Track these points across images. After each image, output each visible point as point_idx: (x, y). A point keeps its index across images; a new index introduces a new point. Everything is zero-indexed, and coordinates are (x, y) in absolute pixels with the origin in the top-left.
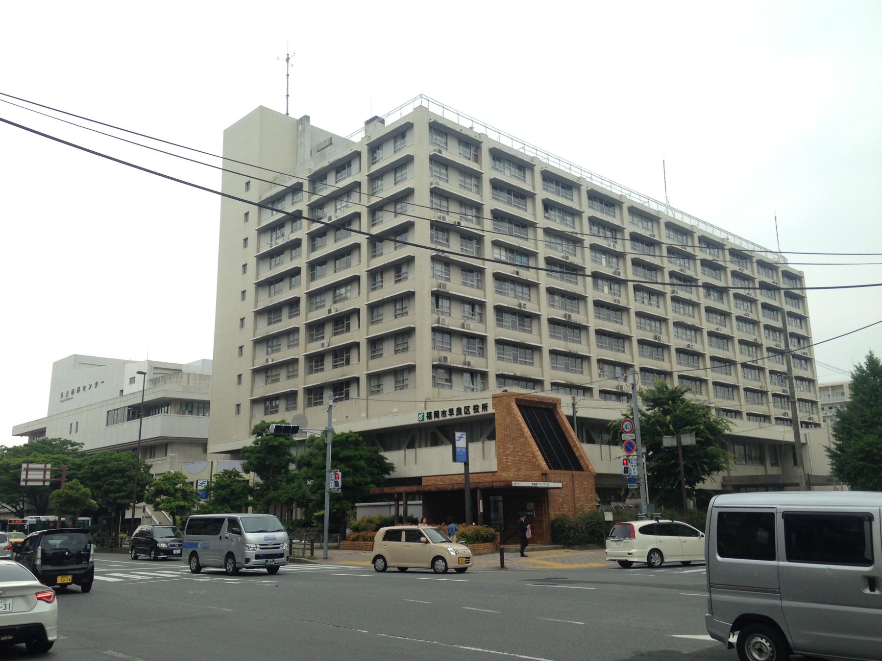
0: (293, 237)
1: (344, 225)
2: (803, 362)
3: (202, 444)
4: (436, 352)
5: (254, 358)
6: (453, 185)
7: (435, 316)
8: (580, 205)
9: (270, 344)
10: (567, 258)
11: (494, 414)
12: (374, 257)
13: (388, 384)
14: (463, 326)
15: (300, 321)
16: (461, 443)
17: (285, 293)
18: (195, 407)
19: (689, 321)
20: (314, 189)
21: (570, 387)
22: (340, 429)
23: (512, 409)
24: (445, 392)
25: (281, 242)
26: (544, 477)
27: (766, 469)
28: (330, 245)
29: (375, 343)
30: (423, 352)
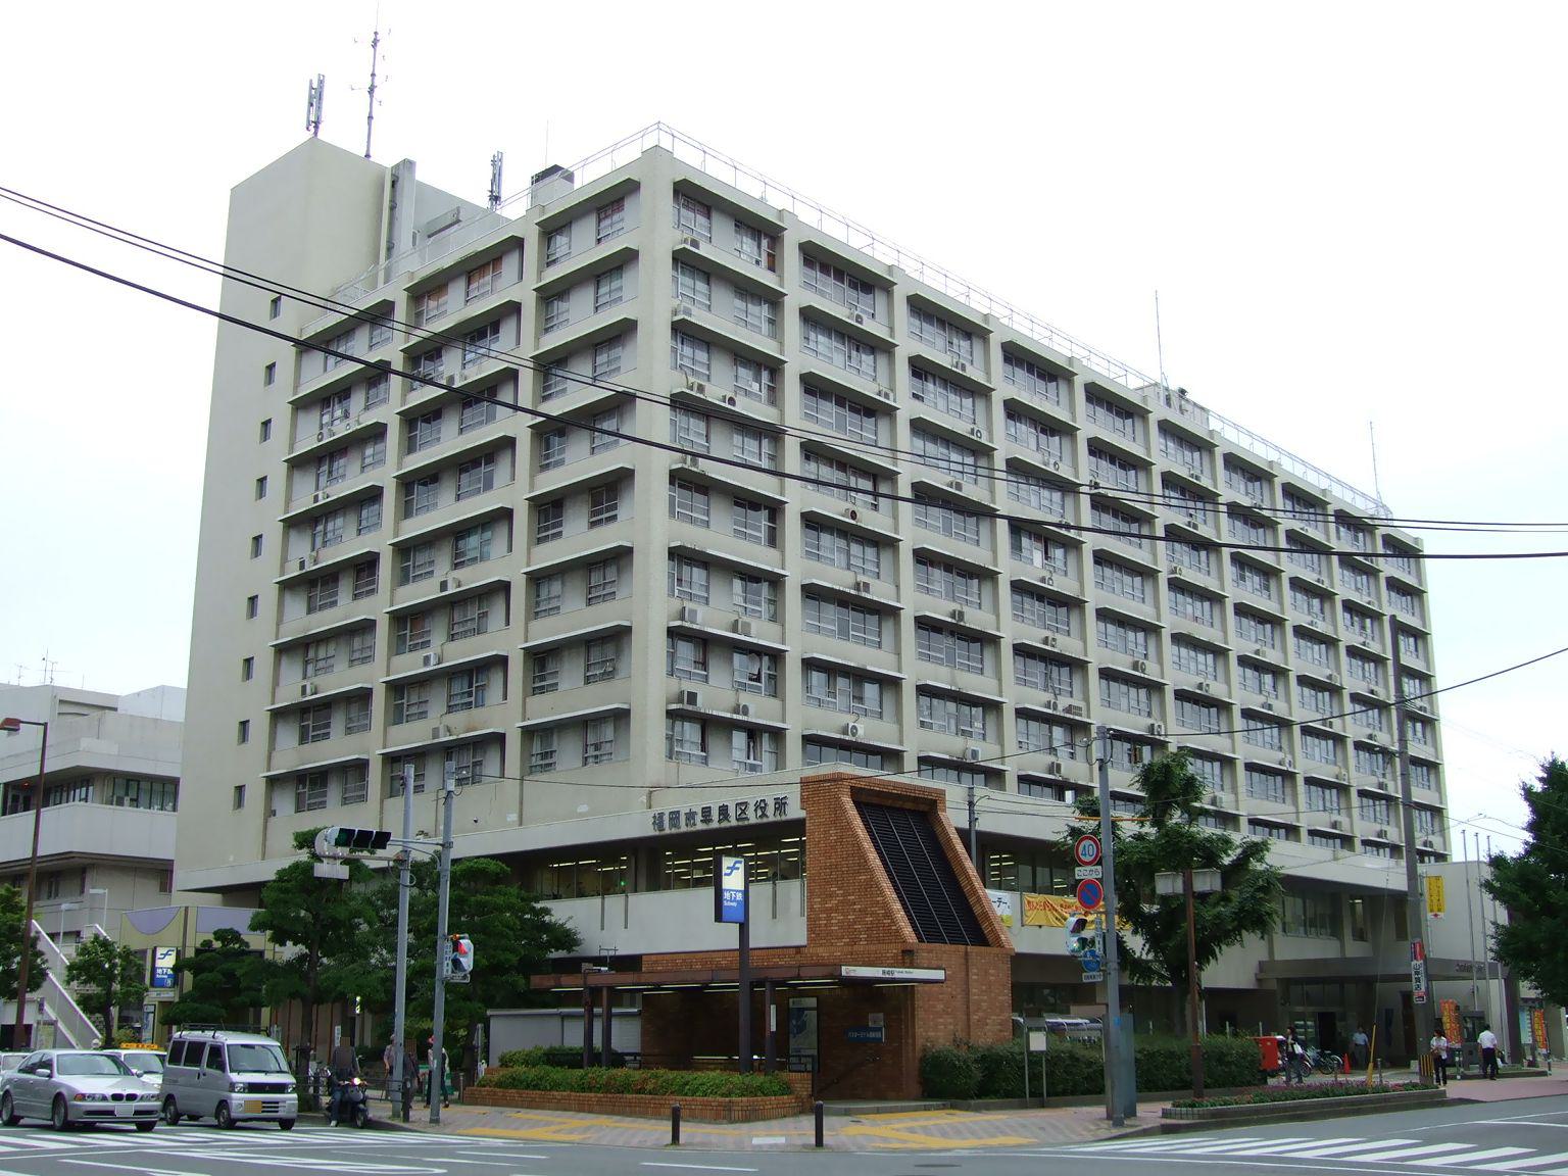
0: (369, 419)
1: (483, 394)
2: (1419, 726)
3: (160, 872)
4: (674, 681)
5: (276, 683)
6: (723, 316)
7: (676, 604)
8: (988, 373)
9: (311, 654)
10: (959, 486)
11: (804, 820)
12: (545, 468)
13: (568, 752)
14: (734, 628)
15: (378, 606)
16: (733, 879)
17: (347, 544)
18: (156, 790)
19: (1203, 633)
20: (419, 315)
21: (961, 767)
22: (471, 845)
23: (845, 811)
24: (693, 772)
25: (341, 430)
26: (907, 957)
27: (1343, 946)
28: (450, 440)
29: (541, 659)
30: (649, 680)
